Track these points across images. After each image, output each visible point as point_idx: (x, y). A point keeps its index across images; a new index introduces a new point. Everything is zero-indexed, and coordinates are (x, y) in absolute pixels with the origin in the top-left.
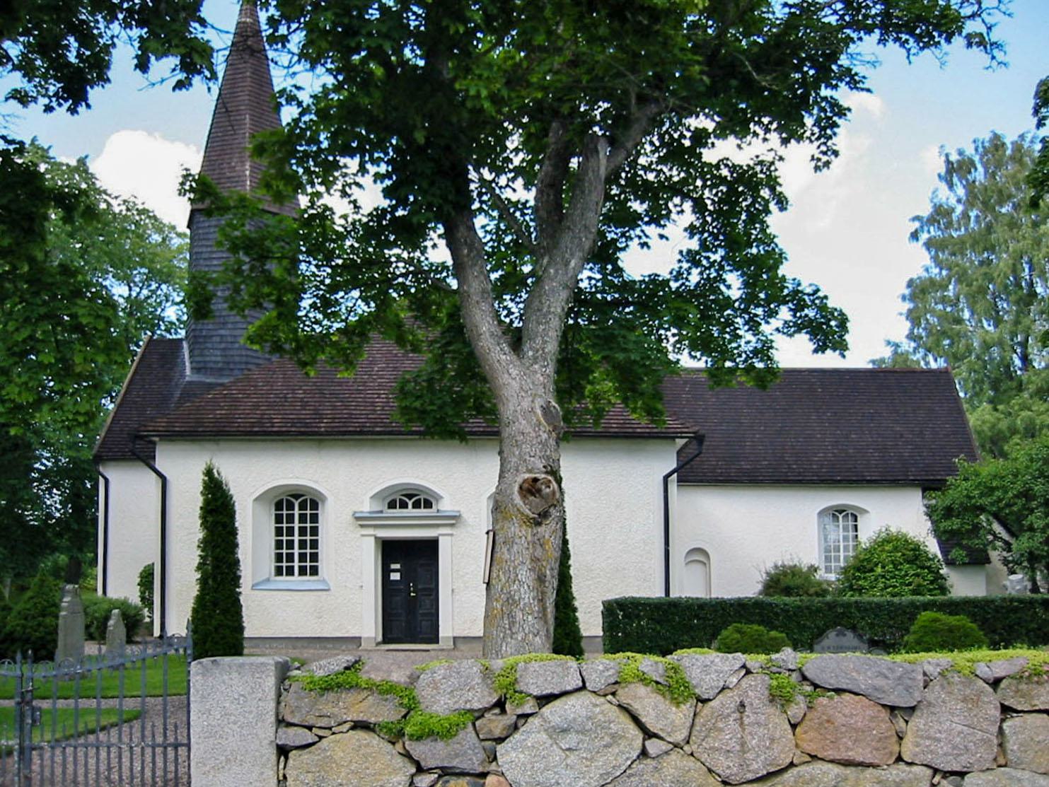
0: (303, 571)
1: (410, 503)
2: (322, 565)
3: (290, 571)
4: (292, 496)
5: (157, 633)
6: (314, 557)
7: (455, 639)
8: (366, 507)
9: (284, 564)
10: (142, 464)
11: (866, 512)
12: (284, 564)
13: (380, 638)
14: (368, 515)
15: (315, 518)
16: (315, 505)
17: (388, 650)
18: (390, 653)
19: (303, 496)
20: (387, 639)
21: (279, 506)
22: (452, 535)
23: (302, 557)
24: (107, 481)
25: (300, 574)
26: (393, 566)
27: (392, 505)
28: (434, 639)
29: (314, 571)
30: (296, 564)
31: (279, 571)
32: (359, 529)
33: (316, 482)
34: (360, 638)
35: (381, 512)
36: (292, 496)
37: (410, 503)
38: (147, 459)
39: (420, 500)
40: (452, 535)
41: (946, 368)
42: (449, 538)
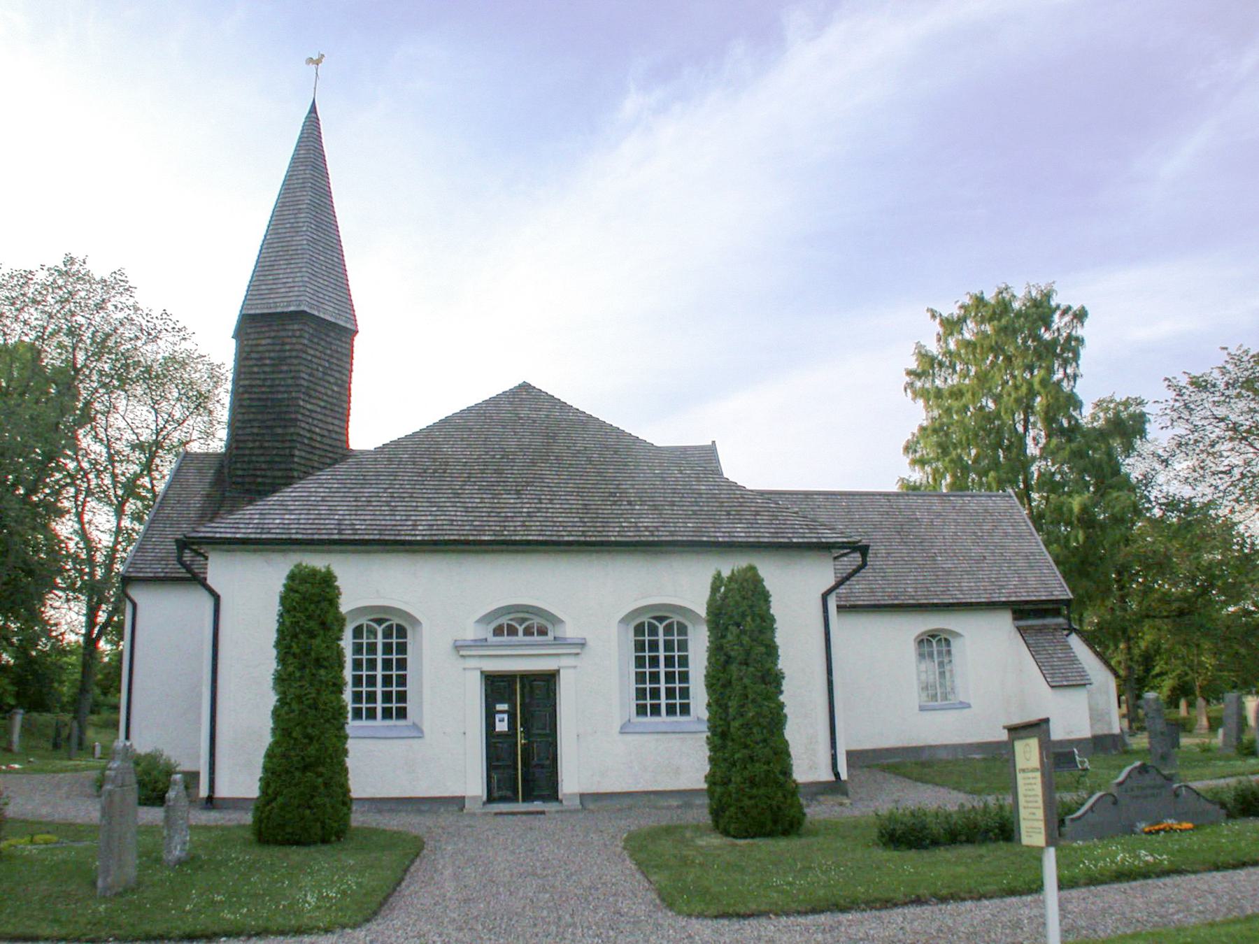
0: (671, 710)
1: (521, 629)
2: (410, 706)
3: (656, 710)
4: (655, 618)
5: (203, 792)
6: (402, 697)
7: (583, 796)
8: (471, 632)
9: (364, 706)
10: (200, 587)
11: (957, 635)
12: (364, 706)
13: (485, 798)
14: (472, 643)
15: (402, 648)
16: (402, 632)
17: (496, 814)
18: (499, 819)
19: (387, 620)
20: (490, 799)
21: (639, 630)
22: (575, 667)
23: (387, 697)
24: (135, 606)
25: (668, 713)
26: (500, 707)
27: (498, 631)
28: (552, 793)
29: (402, 713)
30: (379, 705)
31: (641, 710)
32: (461, 661)
33: (406, 603)
34: (463, 798)
35: (486, 640)
36: (655, 618)
37: (521, 629)
38: (196, 579)
39: (392, 625)
40: (575, 667)
41: (338, 451)
42: (572, 671)
